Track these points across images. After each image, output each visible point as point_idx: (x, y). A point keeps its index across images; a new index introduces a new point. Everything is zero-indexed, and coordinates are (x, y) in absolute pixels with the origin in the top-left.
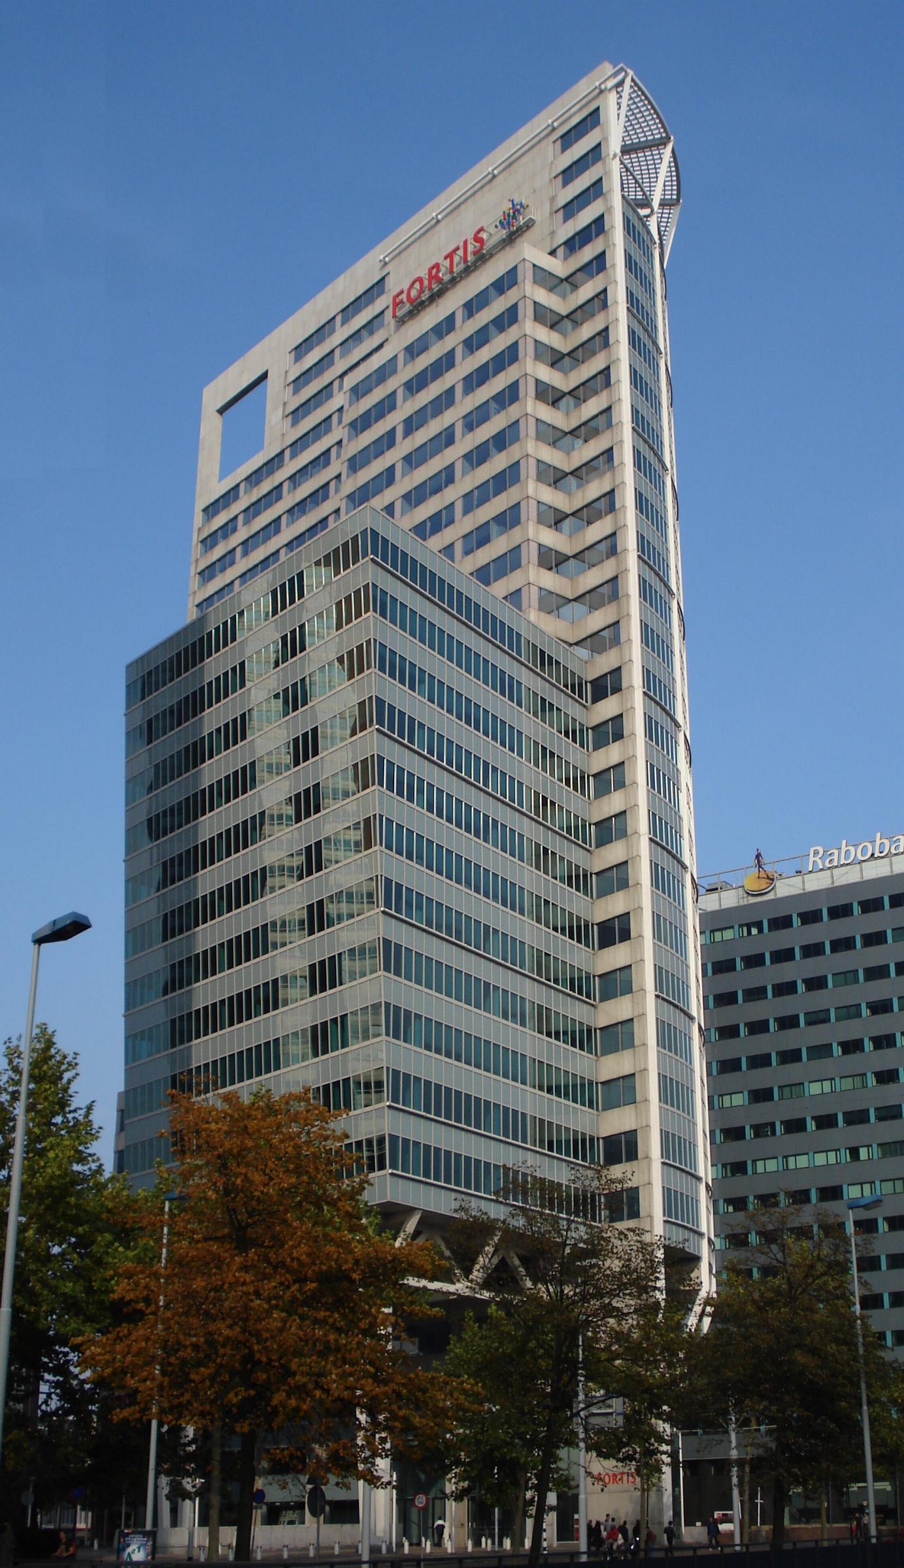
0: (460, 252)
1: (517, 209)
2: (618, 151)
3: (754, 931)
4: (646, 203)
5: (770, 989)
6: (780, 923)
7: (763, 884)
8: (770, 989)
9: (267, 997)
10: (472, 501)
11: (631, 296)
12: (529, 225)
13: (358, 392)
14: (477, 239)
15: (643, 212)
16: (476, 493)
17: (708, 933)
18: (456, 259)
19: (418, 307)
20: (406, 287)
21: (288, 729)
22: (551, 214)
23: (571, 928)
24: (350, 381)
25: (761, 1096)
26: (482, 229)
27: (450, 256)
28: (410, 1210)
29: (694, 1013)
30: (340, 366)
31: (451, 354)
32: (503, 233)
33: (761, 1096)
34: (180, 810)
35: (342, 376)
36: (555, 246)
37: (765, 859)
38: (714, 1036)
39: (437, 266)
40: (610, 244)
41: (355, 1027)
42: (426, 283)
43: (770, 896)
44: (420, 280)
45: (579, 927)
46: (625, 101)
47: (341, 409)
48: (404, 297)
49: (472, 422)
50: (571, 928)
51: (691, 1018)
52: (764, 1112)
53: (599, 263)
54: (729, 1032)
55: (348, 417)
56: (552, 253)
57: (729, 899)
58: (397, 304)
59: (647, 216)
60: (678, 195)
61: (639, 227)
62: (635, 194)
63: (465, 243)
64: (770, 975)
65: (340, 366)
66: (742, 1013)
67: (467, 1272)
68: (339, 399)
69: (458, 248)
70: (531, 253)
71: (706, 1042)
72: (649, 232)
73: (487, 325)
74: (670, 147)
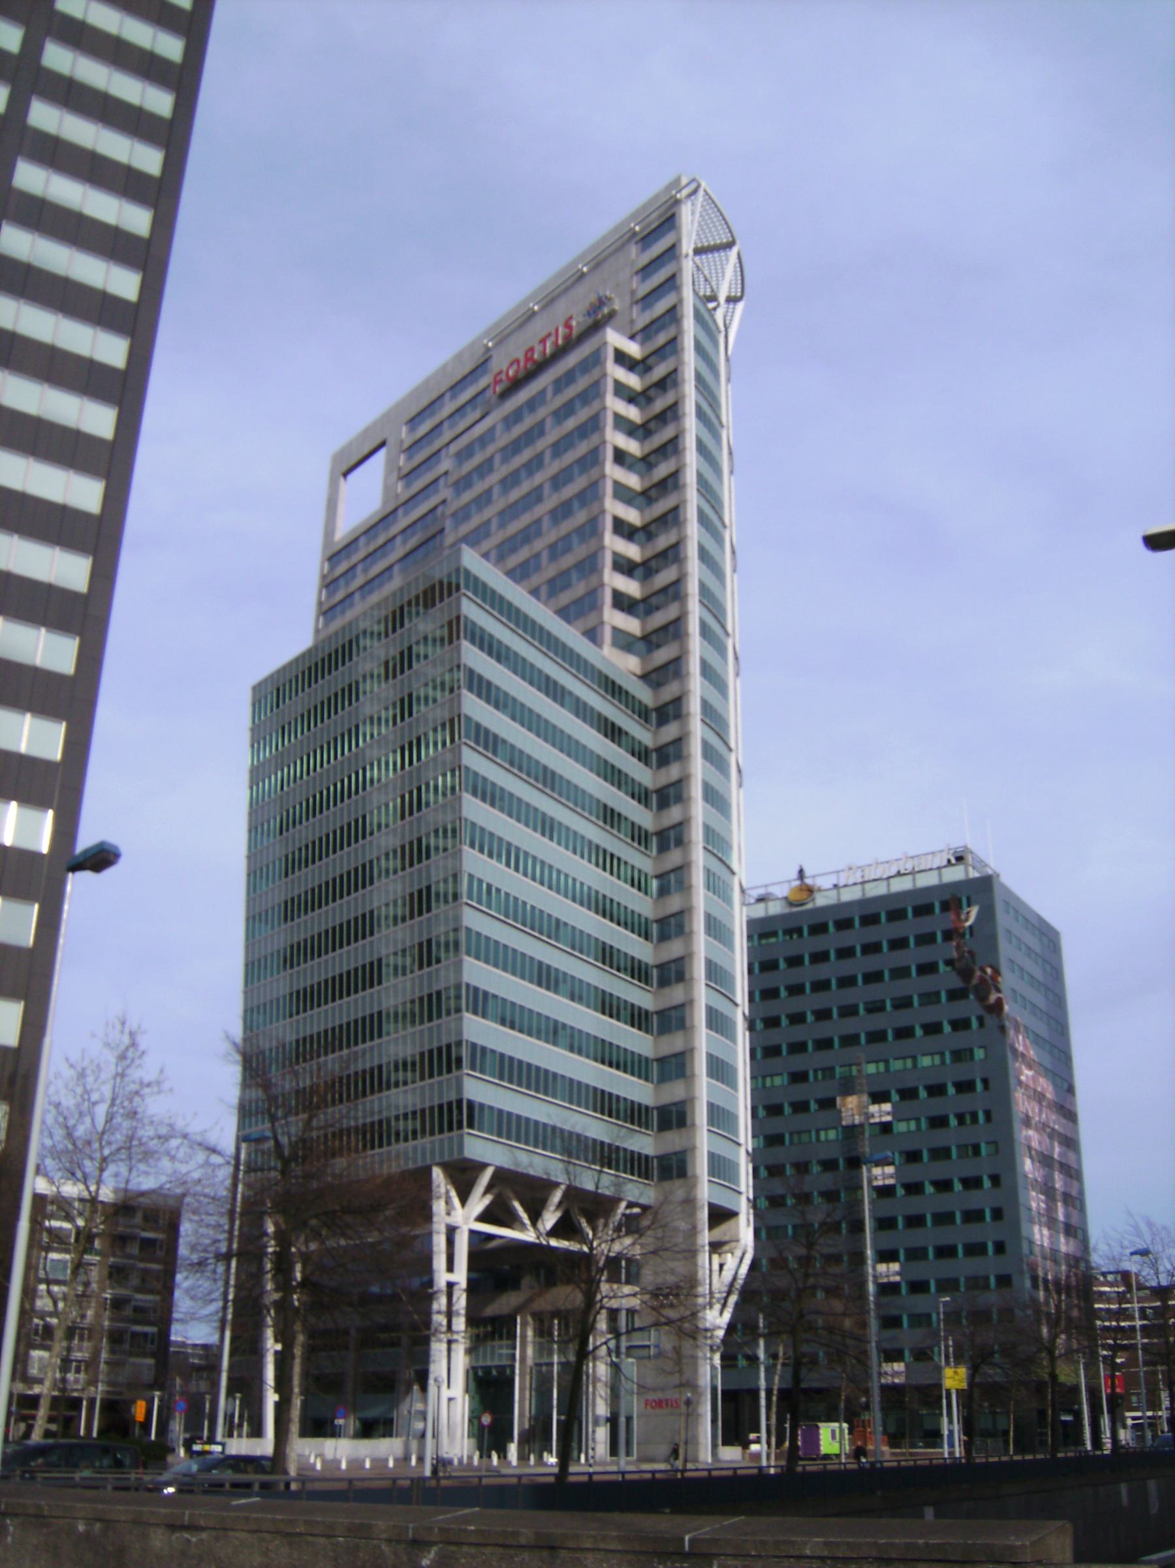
0: (553, 338)
1: (602, 302)
2: (691, 253)
3: (795, 936)
4: (713, 298)
5: (808, 990)
6: (819, 929)
7: (804, 895)
8: (808, 990)
9: (371, 974)
10: (558, 448)
11: (699, 378)
12: (612, 315)
13: (464, 455)
14: (568, 325)
15: (711, 305)
16: (560, 544)
17: (756, 937)
18: (548, 344)
19: (516, 384)
20: (505, 369)
21: (404, 883)
22: (632, 305)
23: (633, 924)
24: (453, 448)
25: (799, 1077)
26: (571, 318)
27: (543, 341)
28: (483, 1166)
29: (739, 1000)
30: (447, 435)
31: (542, 423)
32: (590, 321)
33: (799, 1077)
34: (326, 1048)
35: (448, 444)
36: (634, 331)
37: (807, 872)
38: (759, 1025)
39: (532, 350)
40: (680, 362)
41: (438, 895)
42: (522, 364)
43: (809, 906)
44: (518, 361)
45: (633, 1063)
46: (699, 209)
47: (446, 473)
48: (504, 377)
49: (558, 448)
50: (633, 924)
51: (736, 1005)
52: (800, 1092)
53: (673, 345)
54: (772, 1022)
55: (452, 478)
56: (632, 337)
57: (775, 908)
58: (497, 382)
59: (715, 309)
60: (743, 291)
61: (706, 316)
62: (705, 290)
63: (557, 330)
64: (808, 973)
65: (447, 435)
66: (785, 1005)
67: (535, 1216)
68: (446, 464)
69: (549, 335)
70: (614, 338)
71: (751, 1027)
72: (715, 321)
73: (571, 499)
74: (735, 250)
